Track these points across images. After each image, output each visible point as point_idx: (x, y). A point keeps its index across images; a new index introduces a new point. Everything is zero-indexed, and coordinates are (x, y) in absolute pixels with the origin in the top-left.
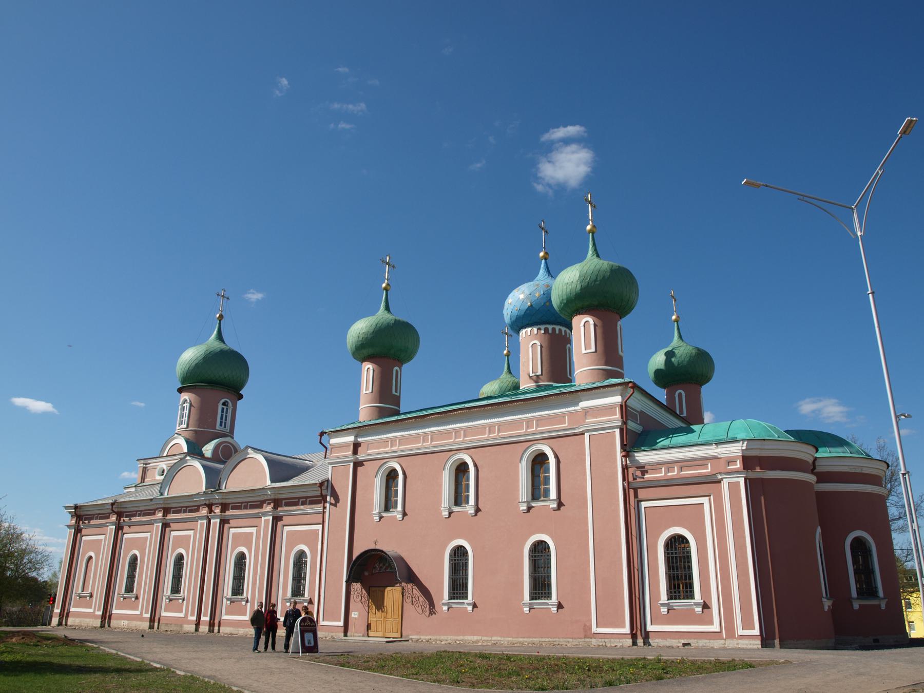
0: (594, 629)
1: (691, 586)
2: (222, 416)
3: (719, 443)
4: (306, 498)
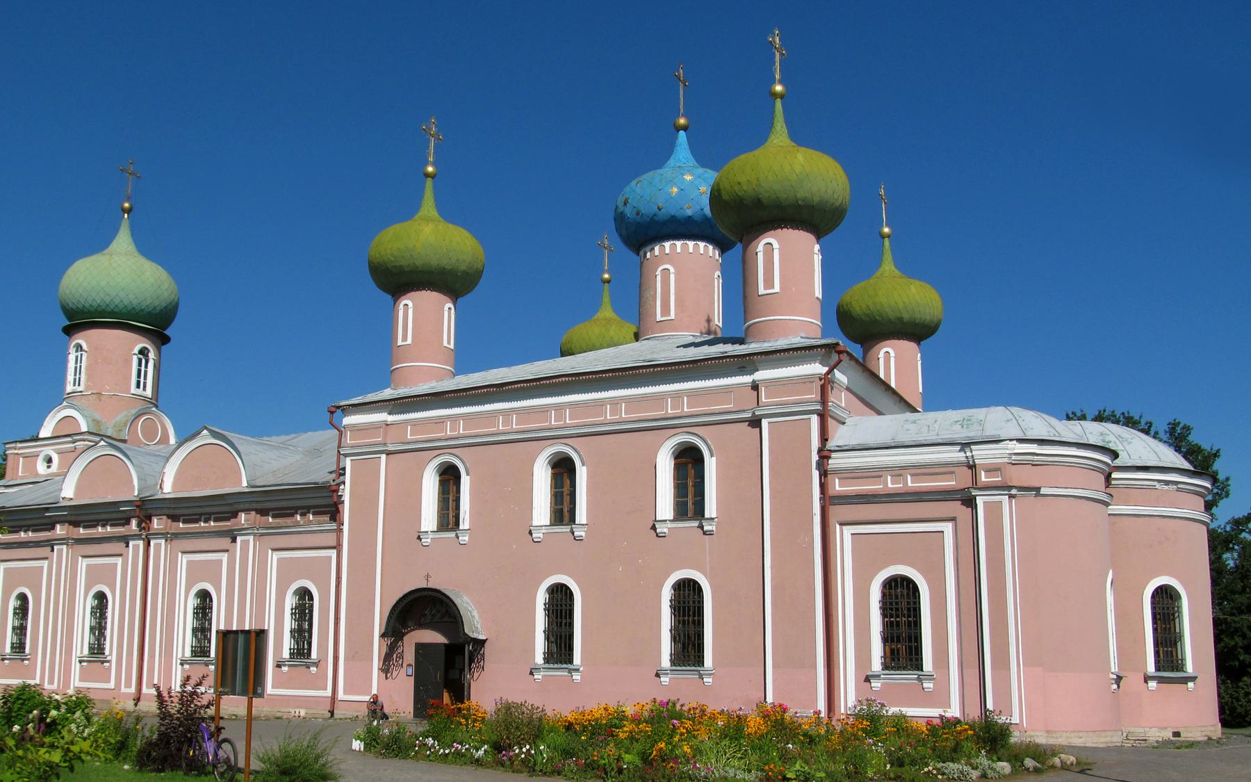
0: (112, 685)
1: (571, 648)
2: (139, 371)
3: (1041, 442)
4: (210, 514)
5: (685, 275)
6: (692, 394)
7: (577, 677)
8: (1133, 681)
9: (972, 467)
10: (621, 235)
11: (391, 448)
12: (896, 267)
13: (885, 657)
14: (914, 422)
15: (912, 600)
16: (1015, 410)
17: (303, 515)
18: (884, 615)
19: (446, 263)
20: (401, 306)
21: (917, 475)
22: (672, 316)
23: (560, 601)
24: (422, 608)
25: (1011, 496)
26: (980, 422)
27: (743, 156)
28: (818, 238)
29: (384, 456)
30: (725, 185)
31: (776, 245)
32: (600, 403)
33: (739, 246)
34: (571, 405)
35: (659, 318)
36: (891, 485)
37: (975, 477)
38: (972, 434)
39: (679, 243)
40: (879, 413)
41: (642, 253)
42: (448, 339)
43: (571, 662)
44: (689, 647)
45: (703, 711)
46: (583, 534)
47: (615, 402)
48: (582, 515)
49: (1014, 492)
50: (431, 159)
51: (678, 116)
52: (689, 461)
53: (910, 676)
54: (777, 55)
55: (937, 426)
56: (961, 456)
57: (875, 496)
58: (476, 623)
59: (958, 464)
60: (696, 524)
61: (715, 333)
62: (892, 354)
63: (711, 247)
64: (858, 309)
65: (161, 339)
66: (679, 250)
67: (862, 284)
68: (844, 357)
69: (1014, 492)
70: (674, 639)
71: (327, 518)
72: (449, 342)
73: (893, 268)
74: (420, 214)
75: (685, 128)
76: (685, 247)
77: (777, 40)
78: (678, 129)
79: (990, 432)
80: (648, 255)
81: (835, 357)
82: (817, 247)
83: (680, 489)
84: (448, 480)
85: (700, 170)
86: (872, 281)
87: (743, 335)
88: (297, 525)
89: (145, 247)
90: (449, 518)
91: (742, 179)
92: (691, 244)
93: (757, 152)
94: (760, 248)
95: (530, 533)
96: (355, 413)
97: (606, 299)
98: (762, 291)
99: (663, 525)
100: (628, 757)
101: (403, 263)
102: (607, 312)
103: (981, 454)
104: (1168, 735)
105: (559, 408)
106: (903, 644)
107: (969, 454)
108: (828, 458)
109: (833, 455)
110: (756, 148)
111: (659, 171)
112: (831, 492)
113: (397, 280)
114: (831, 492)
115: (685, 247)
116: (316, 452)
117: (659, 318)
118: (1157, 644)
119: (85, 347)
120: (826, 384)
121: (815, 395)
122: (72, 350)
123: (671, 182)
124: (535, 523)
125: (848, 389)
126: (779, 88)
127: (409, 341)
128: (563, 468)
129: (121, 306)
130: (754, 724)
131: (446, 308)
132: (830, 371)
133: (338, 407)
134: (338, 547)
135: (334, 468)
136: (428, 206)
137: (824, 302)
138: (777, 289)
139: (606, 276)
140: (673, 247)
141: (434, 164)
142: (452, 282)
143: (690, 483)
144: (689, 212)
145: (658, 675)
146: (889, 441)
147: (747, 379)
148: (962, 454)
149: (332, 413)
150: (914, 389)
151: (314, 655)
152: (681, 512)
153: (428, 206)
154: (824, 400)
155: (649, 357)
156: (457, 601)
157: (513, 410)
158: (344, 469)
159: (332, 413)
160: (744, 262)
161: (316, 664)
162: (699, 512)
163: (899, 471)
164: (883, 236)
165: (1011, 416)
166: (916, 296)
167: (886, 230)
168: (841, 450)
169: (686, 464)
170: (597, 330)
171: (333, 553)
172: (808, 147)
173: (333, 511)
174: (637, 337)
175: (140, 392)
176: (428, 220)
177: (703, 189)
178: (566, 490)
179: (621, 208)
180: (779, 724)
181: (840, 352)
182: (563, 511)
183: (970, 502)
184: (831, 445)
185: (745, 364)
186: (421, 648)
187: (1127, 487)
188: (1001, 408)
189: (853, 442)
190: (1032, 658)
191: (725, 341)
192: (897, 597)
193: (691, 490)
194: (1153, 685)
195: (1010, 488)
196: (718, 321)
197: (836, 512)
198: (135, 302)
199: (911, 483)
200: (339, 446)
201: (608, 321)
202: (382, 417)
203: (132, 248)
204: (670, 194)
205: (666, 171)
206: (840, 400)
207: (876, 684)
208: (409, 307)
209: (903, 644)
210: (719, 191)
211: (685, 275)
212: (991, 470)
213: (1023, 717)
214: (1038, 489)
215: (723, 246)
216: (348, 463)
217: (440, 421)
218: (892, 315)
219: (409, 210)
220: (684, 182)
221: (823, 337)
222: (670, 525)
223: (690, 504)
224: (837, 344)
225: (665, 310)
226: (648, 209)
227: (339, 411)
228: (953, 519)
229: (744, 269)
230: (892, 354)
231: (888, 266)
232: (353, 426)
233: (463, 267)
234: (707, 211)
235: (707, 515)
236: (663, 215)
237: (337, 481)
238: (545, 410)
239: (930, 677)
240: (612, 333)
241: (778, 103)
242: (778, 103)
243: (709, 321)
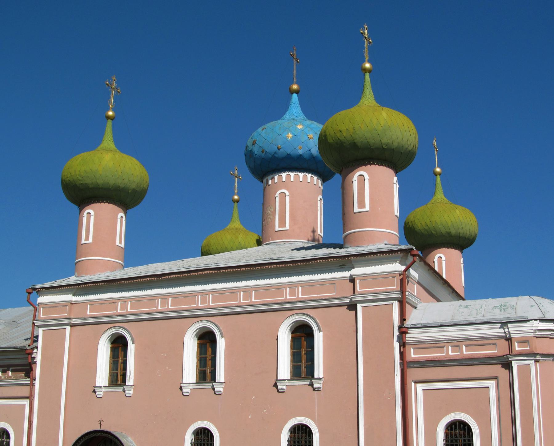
5: (296, 197)
6: (305, 285)
9: (509, 340)
10: (250, 167)
11: (74, 321)
12: (445, 196)
14: (466, 307)
15: (467, 438)
16: (536, 298)
19: (120, 182)
20: (85, 214)
21: (470, 345)
25: (536, 361)
26: (513, 308)
27: (343, 112)
28: (396, 172)
29: (68, 328)
30: (330, 132)
31: (366, 176)
32: (236, 291)
33: (337, 177)
34: (214, 291)
35: (277, 228)
36: (451, 353)
37: (511, 347)
39: (292, 174)
40: (439, 301)
41: (265, 180)
42: (120, 241)
46: (221, 390)
47: (247, 290)
48: (220, 375)
49: (538, 357)
50: (111, 106)
51: (292, 84)
52: (302, 335)
54: (366, 43)
55: (482, 310)
57: (440, 361)
60: (308, 382)
61: (318, 241)
62: (444, 258)
63: (315, 178)
64: (419, 225)
66: (292, 179)
67: (422, 208)
68: (416, 258)
69: (538, 357)
71: (22, 375)
72: (120, 243)
73: (443, 197)
74: (102, 145)
75: (297, 92)
76: (297, 177)
77: (366, 32)
78: (292, 92)
79: (521, 314)
80: (270, 182)
81: (410, 259)
82: (395, 179)
83: (296, 356)
84: (118, 347)
85: (309, 122)
86: (429, 206)
87: (342, 243)
88: (9, 378)
90: (118, 377)
91: (343, 128)
92: (301, 175)
93: (352, 110)
94: (355, 178)
95: (181, 389)
96: (47, 294)
97: (236, 215)
98: (356, 209)
99: (282, 383)
101: (88, 181)
102: (236, 224)
103: (515, 330)
105: (204, 293)
107: (506, 330)
108: (406, 333)
109: (410, 331)
110: (352, 107)
111: (279, 122)
112: (408, 359)
113: (83, 194)
114: (408, 359)
115: (297, 177)
116: (14, 323)
117: (277, 228)
120: (404, 279)
121: (396, 287)
123: (288, 130)
124: (185, 381)
125: (418, 283)
126: (367, 65)
127: (90, 240)
128: (207, 340)
131: (119, 216)
132: (407, 269)
133: (34, 289)
134: (31, 397)
135: (29, 336)
136: (108, 141)
137: (400, 219)
138: (367, 208)
139: (236, 197)
140: (288, 177)
141: (113, 110)
142: (124, 197)
143: (303, 352)
144: (301, 152)
146: (448, 320)
147: (346, 274)
148: (502, 330)
149: (29, 293)
150: (460, 283)
152: (296, 374)
153: (108, 141)
154: (402, 290)
155: (272, 257)
157: (169, 295)
158: (37, 337)
159: (29, 293)
160: (343, 187)
162: (310, 374)
163: (456, 343)
164: (436, 174)
165: (534, 303)
166: (457, 217)
167: (438, 170)
168: (415, 327)
169: (300, 337)
172: (389, 108)
173: (27, 369)
174: (259, 243)
176: (108, 150)
177: (311, 135)
178: (209, 356)
179: (250, 147)
181: (414, 255)
182: (206, 373)
183: (508, 366)
184: (408, 323)
185: (345, 262)
188: (527, 297)
189: (424, 321)
191: (328, 246)
192: (456, 436)
193: (304, 357)
196: (320, 232)
197: (413, 373)
199: (466, 352)
200: (34, 319)
201: (237, 231)
202: (69, 297)
204: (286, 138)
205: (284, 121)
206: (414, 291)
208: (91, 215)
210: (325, 136)
211: (296, 197)
212: (523, 341)
215: (324, 177)
216: (40, 332)
217: (113, 302)
218: (443, 231)
219: (93, 143)
220: (298, 131)
221: (400, 243)
222: (288, 383)
224: (412, 249)
225: (282, 222)
226: (271, 149)
227: (35, 292)
228: (495, 378)
229: (343, 194)
230: (444, 258)
231: (440, 195)
232: (46, 304)
233: (133, 186)
234: (315, 151)
235: (316, 376)
236: (282, 153)
237: (32, 346)
238: (193, 295)
241: (367, 76)
242: (367, 76)
243: (314, 231)
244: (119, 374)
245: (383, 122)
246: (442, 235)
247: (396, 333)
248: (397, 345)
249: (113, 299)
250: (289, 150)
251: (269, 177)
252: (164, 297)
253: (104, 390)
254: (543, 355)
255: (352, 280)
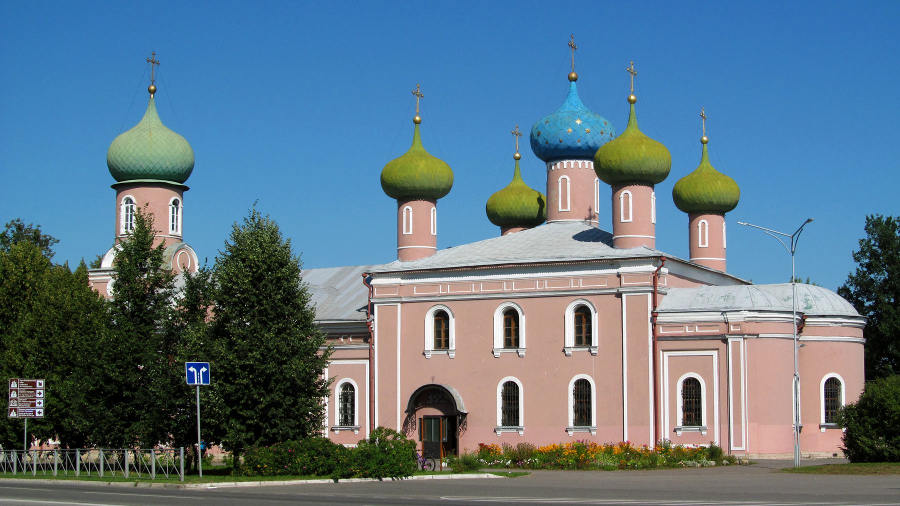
1: (518, 417)
6: (584, 277)
7: (521, 433)
8: (810, 429)
9: (727, 323)
11: (404, 300)
13: (684, 419)
17: (345, 338)
18: (684, 398)
22: (569, 209)
23: (511, 392)
24: (430, 395)
29: (399, 305)
32: (533, 280)
35: (560, 210)
36: (688, 331)
37: (728, 328)
38: (728, 305)
39: (572, 162)
42: (433, 232)
43: (518, 424)
44: (583, 416)
45: (595, 446)
52: (583, 315)
53: (695, 429)
56: (721, 318)
58: (462, 405)
59: (721, 321)
62: (707, 224)
65: (182, 190)
70: (576, 411)
76: (576, 164)
80: (553, 168)
82: (653, 193)
83: (578, 330)
89: (170, 120)
91: (613, 159)
92: (580, 162)
94: (622, 196)
95: (493, 352)
96: (379, 277)
98: (623, 220)
100: (571, 461)
101: (407, 185)
104: (831, 455)
105: (508, 281)
106: (692, 414)
114: (658, 334)
115: (576, 164)
117: (560, 210)
118: (827, 408)
119: (134, 200)
120: (656, 276)
121: (650, 282)
122: (123, 202)
129: (160, 171)
130: (617, 449)
134: (371, 358)
138: (631, 220)
144: (579, 144)
145: (567, 431)
147: (615, 271)
151: (356, 423)
152: (579, 341)
154: (655, 285)
156: (451, 391)
161: (358, 429)
163: (691, 324)
170: (513, 197)
171: (367, 362)
175: (173, 233)
177: (588, 129)
178: (513, 327)
180: (626, 448)
183: (725, 341)
184: (658, 309)
185: (613, 263)
186: (427, 418)
187: (814, 326)
190: (752, 419)
194: (823, 430)
195: (743, 335)
197: (661, 345)
198: (170, 167)
203: (159, 122)
206: (662, 283)
207: (679, 433)
209: (692, 414)
213: (745, 444)
214: (758, 335)
217: (436, 285)
218: (706, 201)
223: (584, 338)
226: (554, 141)
228: (718, 349)
230: (707, 224)
238: (500, 282)
239: (705, 429)
240: (523, 200)
243: (590, 210)
244: (443, 340)
245: (642, 155)
246: (705, 204)
247: (650, 316)
248: (650, 325)
249: (435, 283)
250: (569, 144)
251: (553, 163)
252: (477, 283)
253: (431, 353)
254: (749, 335)
255: (619, 276)
